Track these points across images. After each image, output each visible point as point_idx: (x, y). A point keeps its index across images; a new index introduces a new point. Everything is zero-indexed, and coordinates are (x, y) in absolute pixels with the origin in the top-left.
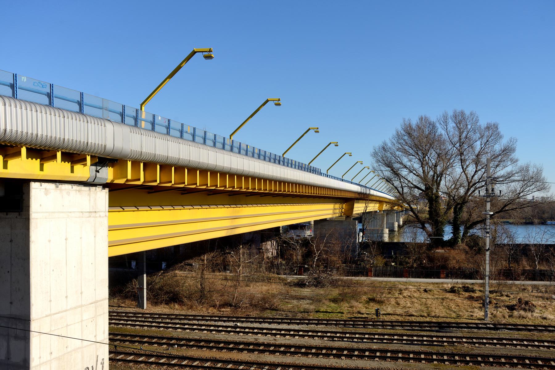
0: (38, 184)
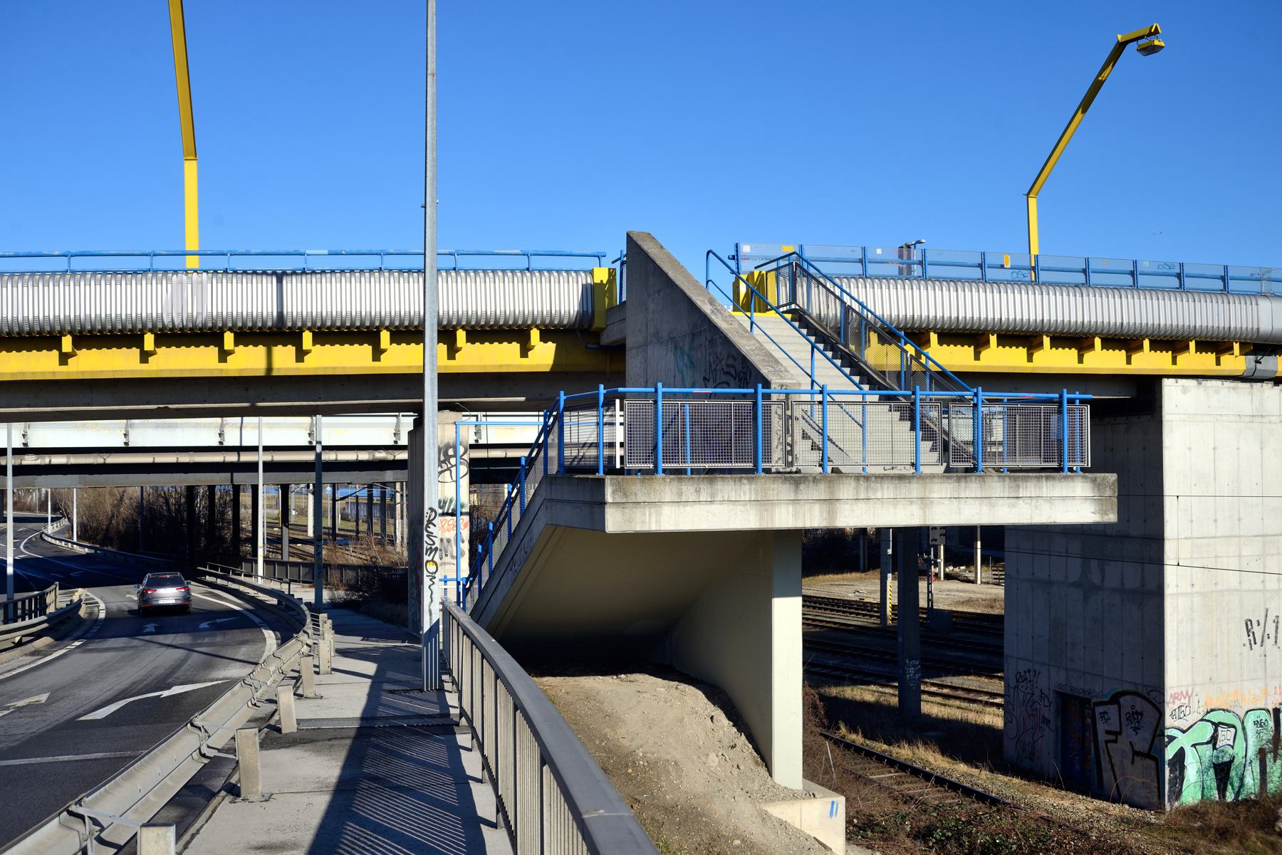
0: (1172, 381)
